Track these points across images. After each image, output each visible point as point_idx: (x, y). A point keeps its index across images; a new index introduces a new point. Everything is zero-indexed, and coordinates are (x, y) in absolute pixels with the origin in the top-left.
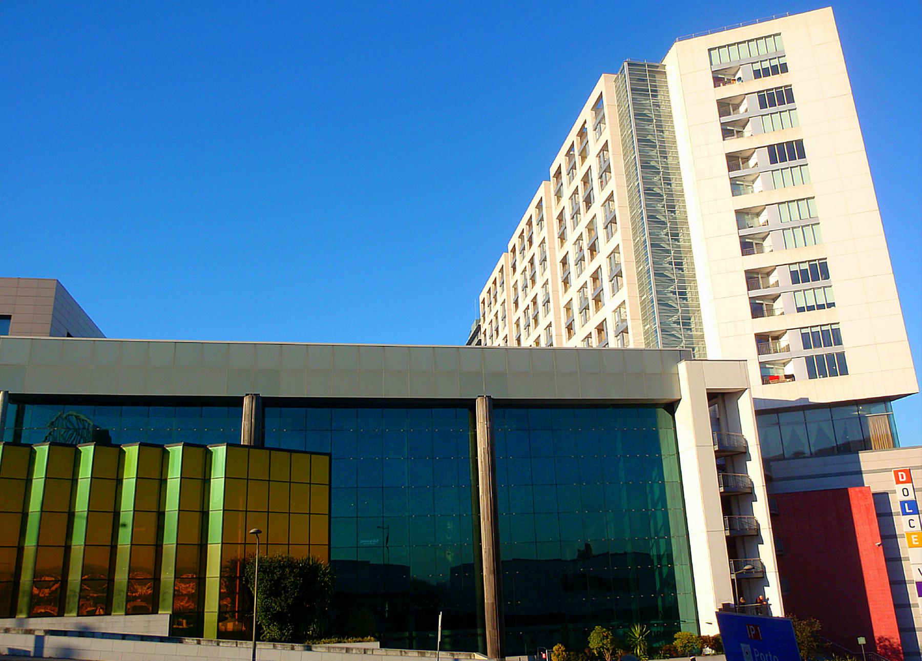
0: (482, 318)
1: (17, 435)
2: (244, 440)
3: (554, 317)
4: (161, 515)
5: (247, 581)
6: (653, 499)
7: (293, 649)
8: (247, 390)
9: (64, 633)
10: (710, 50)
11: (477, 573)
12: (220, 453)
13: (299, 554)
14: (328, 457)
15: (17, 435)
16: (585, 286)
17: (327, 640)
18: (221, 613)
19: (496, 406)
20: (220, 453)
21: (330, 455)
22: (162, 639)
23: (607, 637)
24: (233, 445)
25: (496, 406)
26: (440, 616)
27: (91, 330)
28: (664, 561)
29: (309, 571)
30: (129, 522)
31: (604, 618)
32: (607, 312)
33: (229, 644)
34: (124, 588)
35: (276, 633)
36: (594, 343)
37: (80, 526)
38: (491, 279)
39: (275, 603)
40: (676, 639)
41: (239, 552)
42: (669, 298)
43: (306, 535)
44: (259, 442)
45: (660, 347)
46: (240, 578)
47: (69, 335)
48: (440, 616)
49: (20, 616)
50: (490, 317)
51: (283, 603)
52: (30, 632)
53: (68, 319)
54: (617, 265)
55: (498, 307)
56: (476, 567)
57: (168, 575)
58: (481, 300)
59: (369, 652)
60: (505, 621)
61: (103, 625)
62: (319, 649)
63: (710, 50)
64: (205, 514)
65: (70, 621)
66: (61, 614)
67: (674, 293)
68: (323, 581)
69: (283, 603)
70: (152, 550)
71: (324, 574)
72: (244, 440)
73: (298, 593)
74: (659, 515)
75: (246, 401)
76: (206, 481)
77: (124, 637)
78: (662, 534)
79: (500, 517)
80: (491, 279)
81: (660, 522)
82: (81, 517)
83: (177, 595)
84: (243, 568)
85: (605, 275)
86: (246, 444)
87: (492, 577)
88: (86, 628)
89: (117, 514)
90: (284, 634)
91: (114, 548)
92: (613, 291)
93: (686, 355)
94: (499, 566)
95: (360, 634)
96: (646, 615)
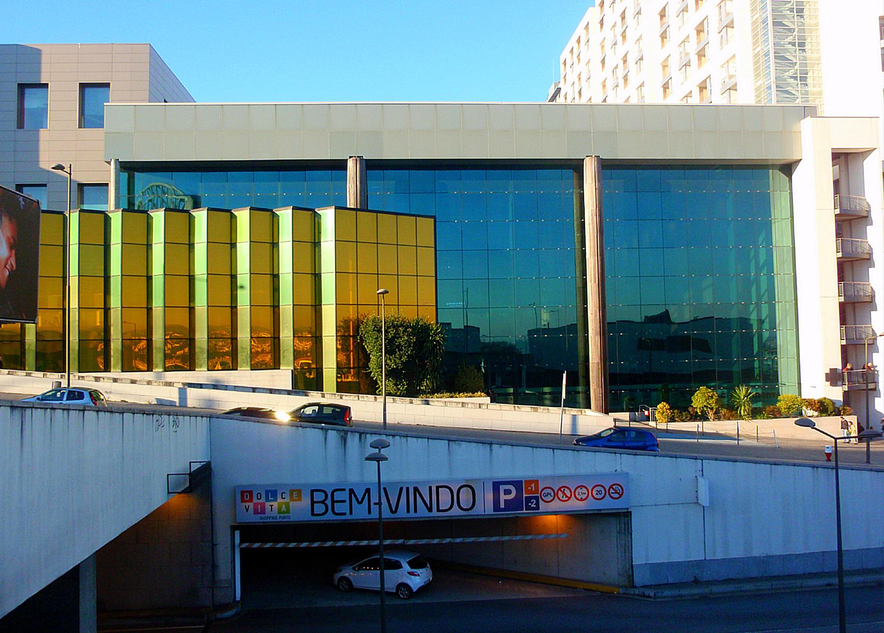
0: (562, 80)
1: (131, 203)
2: (351, 203)
3: (653, 77)
4: (275, 277)
5: (362, 341)
6: (757, 263)
7: (411, 403)
8: (350, 150)
9: (200, 386)
10: (83, 86)
11: (580, 334)
12: (328, 216)
13: (409, 315)
14: (433, 220)
15: (131, 203)
16: (686, 40)
17: (439, 395)
18: (339, 368)
19: (606, 166)
20: (328, 216)
21: (434, 217)
22: (289, 393)
23: (712, 397)
24: (341, 208)
25: (606, 166)
26: (565, 375)
27: (189, 98)
28: (766, 325)
29: (421, 331)
30: (247, 284)
31: (705, 378)
32: (713, 67)
33: (352, 398)
34: (205, 346)
35: (391, 387)
36: (695, 100)
37: (201, 288)
38: (574, 38)
39: (390, 359)
40: (779, 401)
41: (351, 313)
42: (787, 50)
43: (416, 298)
44: (363, 207)
45: (774, 103)
46: (354, 337)
47: (165, 101)
48: (565, 375)
49: (157, 370)
50: (572, 77)
51: (397, 361)
52: (170, 384)
53: (164, 85)
54: (728, 14)
55: (577, 68)
56: (580, 328)
57: (286, 334)
58: (562, 61)
59: (484, 407)
60: (611, 379)
61: (232, 379)
62: (436, 403)
63: (83, 86)
64: (317, 277)
65: (201, 375)
66: (192, 368)
67: (794, 45)
68: (434, 340)
69: (397, 361)
70: (269, 310)
71: (436, 334)
72: (351, 203)
73: (412, 351)
74: (763, 280)
75: (351, 164)
76: (316, 244)
77: (254, 390)
78: (765, 298)
79: (606, 279)
80: (574, 38)
81: (764, 287)
82: (201, 280)
83: (297, 354)
84: (357, 328)
85: (713, 26)
86: (352, 207)
87: (598, 338)
88: (217, 381)
89: (234, 277)
90: (399, 389)
91: (234, 308)
92: (721, 43)
93: (809, 111)
94: (606, 327)
95: (469, 389)
96: (747, 377)
